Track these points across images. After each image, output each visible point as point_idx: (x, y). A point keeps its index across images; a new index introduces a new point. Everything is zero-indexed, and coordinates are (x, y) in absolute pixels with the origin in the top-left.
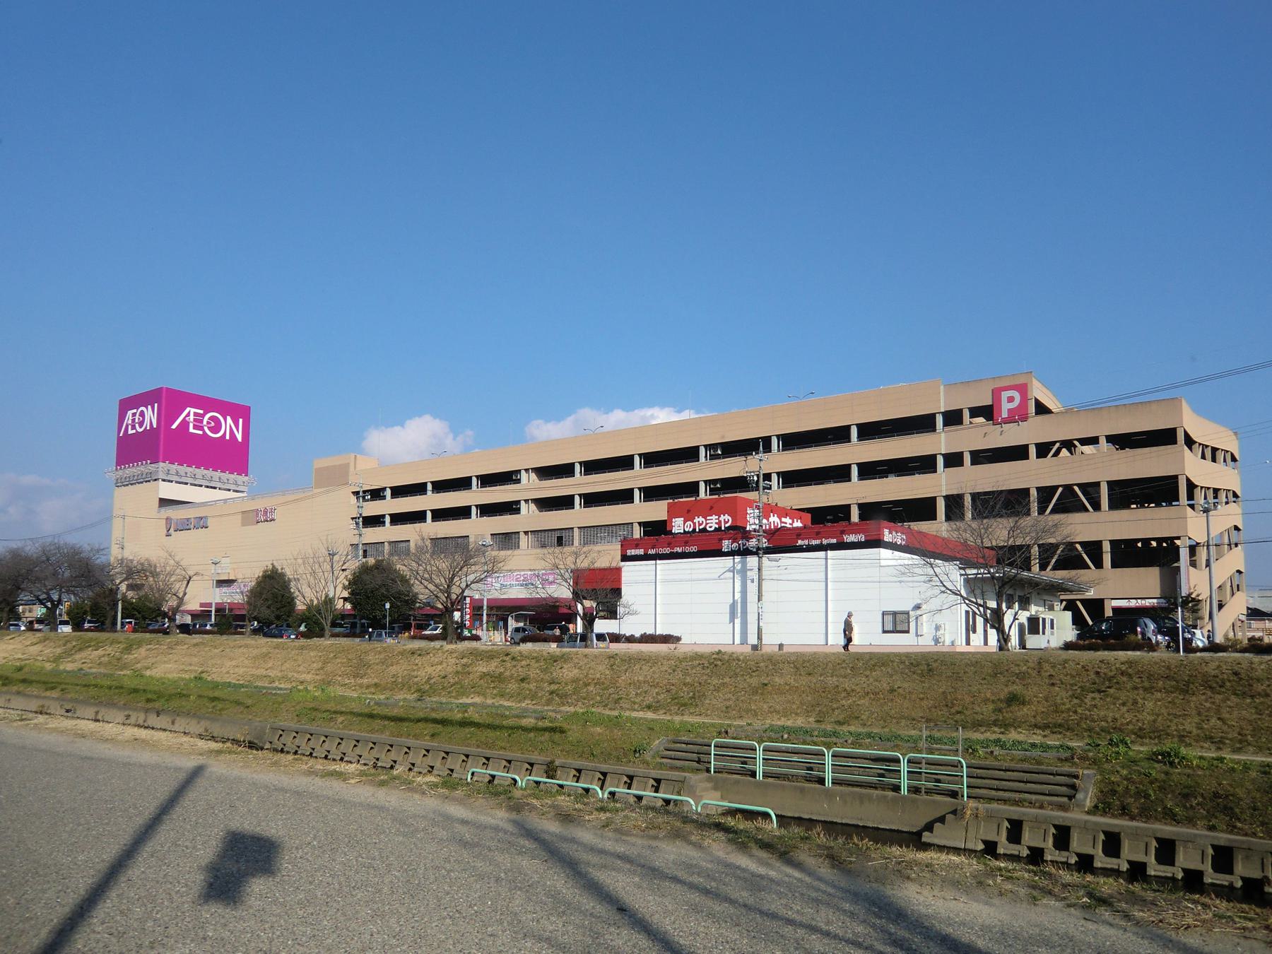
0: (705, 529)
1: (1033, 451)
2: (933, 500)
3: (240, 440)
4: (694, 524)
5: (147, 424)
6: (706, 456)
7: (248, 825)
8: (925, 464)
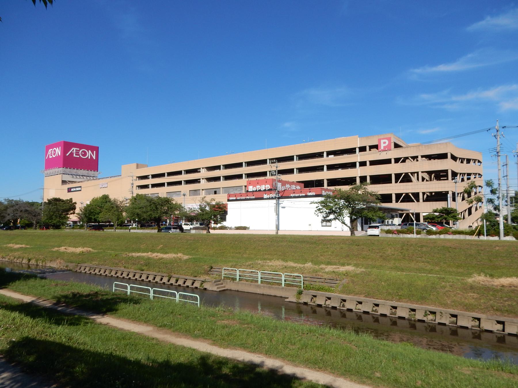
0: (260, 190)
1: (393, 161)
2: (366, 176)
3: (94, 158)
4: (257, 188)
5: (57, 154)
6: (270, 162)
8: (352, 165)
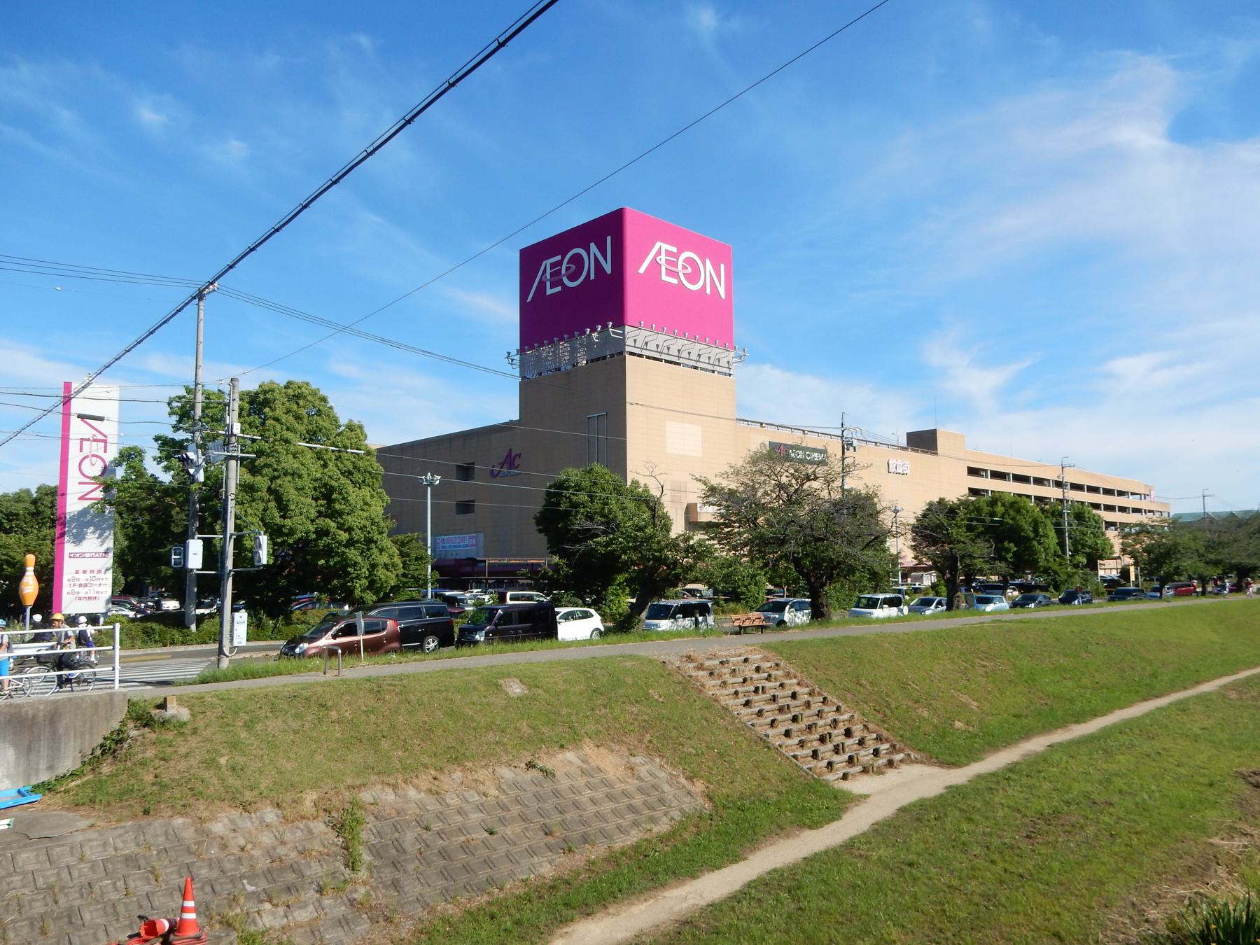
3: (723, 296)
7: (468, 516)
